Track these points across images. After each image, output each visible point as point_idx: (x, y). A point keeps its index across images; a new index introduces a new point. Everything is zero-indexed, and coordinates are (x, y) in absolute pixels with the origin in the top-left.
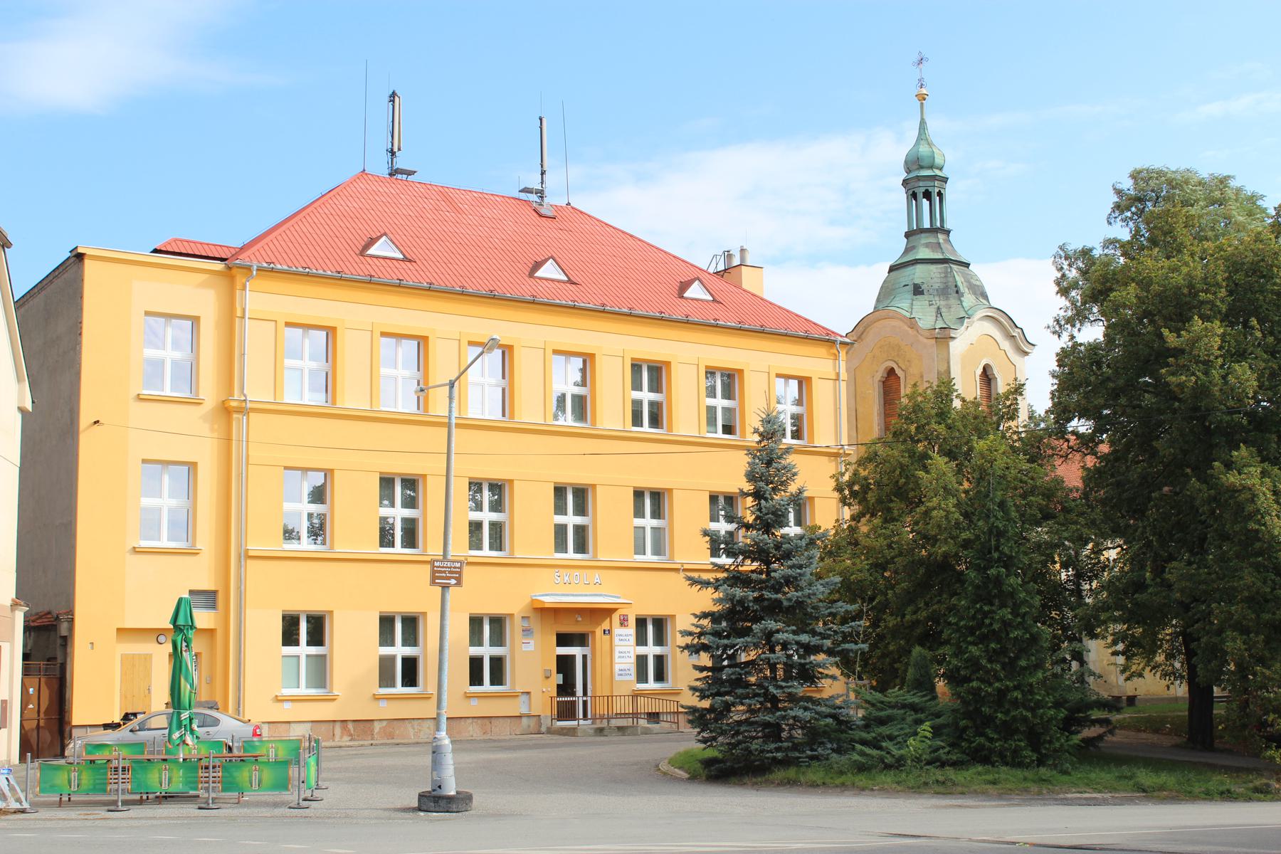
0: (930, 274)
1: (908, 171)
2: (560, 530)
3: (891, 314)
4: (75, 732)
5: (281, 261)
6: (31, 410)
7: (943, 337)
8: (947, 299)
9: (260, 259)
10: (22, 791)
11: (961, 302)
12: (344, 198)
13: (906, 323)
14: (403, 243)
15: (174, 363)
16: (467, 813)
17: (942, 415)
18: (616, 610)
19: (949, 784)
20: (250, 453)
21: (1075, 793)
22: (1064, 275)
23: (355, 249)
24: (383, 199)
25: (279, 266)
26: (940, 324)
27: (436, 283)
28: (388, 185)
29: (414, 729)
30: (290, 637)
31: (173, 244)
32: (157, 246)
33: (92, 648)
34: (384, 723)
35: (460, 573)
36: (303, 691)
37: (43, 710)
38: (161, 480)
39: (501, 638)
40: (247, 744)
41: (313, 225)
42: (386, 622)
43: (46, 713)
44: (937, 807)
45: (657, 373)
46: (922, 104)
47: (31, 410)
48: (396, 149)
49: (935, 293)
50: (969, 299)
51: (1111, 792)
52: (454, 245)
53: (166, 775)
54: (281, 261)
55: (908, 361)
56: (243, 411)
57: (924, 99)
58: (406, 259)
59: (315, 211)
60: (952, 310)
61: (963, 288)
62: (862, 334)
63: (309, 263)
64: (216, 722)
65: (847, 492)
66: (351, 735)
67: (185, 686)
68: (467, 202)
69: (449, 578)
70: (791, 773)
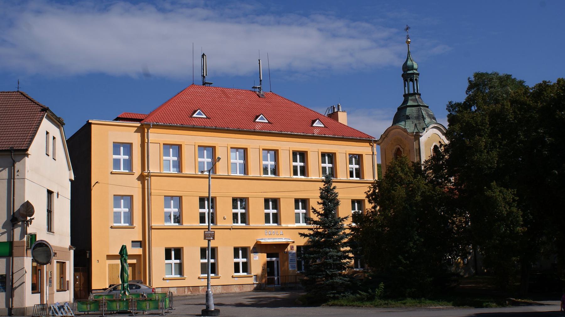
0: (412, 111)
1: (404, 71)
2: (267, 215)
3: (398, 127)
4: (93, 292)
5: (161, 121)
6: (74, 180)
7: (417, 136)
8: (419, 120)
11: (424, 121)
12: (186, 95)
13: (403, 130)
16: (218, 316)
19: (389, 304)
20: (152, 191)
22: (451, 113)
24: (200, 94)
25: (160, 124)
26: (416, 131)
27: (218, 126)
30: (168, 257)
31: (125, 115)
32: (119, 115)
34: (203, 287)
35: (214, 235)
36: (173, 276)
37: (81, 284)
38: (176, 171)
39: (246, 255)
40: (149, 294)
42: (236, 250)
43: (83, 285)
44: (381, 312)
45: (303, 156)
46: (408, 45)
47: (74, 180)
48: (205, 75)
49: (415, 118)
50: (427, 120)
51: (446, 306)
53: (118, 305)
54: (161, 121)
55: (405, 145)
56: (149, 175)
57: (409, 43)
58: (207, 118)
60: (421, 125)
61: (425, 116)
63: (172, 122)
64: (139, 287)
65: (371, 198)
66: (191, 292)
67: (125, 275)
69: (210, 237)
70: (336, 302)
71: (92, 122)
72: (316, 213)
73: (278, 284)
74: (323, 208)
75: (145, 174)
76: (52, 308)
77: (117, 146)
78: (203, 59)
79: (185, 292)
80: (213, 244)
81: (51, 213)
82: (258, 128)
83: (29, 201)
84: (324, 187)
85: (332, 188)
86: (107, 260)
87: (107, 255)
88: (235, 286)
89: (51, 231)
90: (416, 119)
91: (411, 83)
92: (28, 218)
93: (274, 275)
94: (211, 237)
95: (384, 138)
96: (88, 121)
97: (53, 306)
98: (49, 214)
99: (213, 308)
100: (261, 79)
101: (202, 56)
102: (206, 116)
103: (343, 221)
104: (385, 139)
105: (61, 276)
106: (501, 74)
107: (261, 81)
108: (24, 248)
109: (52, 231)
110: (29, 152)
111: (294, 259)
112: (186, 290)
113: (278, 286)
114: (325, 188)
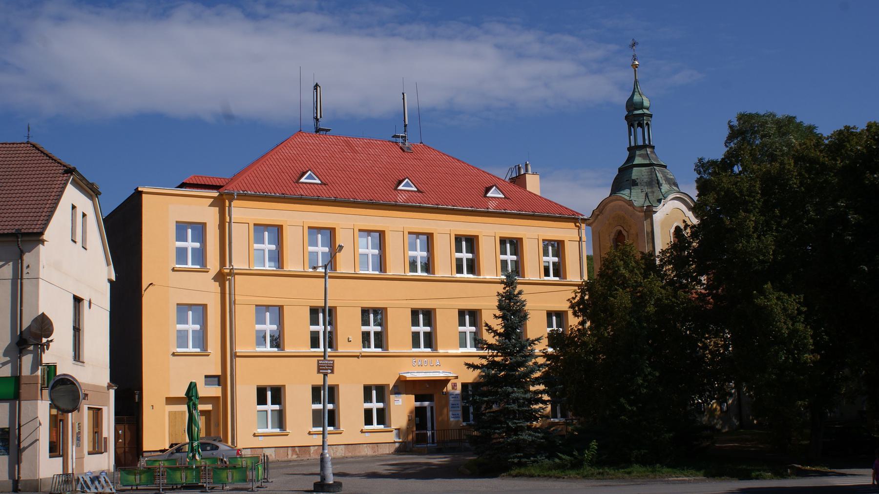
0: (642, 173)
2: (416, 336)
4: (145, 454)
5: (251, 189)
6: (115, 280)
7: (649, 213)
8: (652, 188)
9: (239, 188)
10: (111, 482)
11: (660, 189)
13: (627, 203)
14: (321, 174)
15: (193, 249)
16: (338, 493)
17: (503, 296)
18: (449, 380)
19: (605, 474)
20: (236, 298)
21: (674, 477)
23: (293, 179)
25: (249, 192)
28: (314, 138)
29: (333, 450)
30: (261, 400)
31: (193, 179)
33: (153, 409)
34: (316, 447)
35: (333, 367)
36: (270, 430)
37: (127, 442)
41: (270, 166)
42: (367, 390)
45: (472, 242)
46: (635, 70)
47: (115, 280)
48: (319, 117)
50: (665, 187)
51: (694, 476)
52: (351, 173)
54: (251, 189)
56: (232, 273)
58: (323, 184)
59: (271, 157)
60: (655, 194)
61: (662, 181)
62: (603, 209)
64: (217, 448)
65: (577, 309)
66: (297, 454)
67: (195, 429)
68: (361, 146)
69: (327, 369)
70: (522, 470)
71: (144, 191)
72: (491, 332)
73: (433, 442)
74: (503, 324)
75: (225, 271)
76: (81, 480)
77: (181, 228)
78: (315, 93)
79: (288, 454)
80: (331, 380)
81: (79, 332)
82: (401, 199)
83: (45, 313)
84: (504, 291)
85: (516, 292)
86: (166, 404)
87: (166, 398)
88: (366, 445)
89: (79, 361)
90: (647, 186)
91: (639, 130)
92: (44, 340)
93: (426, 429)
94: (329, 369)
95: (598, 215)
96: (137, 188)
97: (82, 477)
98: (77, 333)
99: (331, 480)
100: (407, 123)
101: (315, 87)
102: (321, 181)
103: (534, 344)
104: (599, 217)
105: (95, 431)
106: (780, 115)
107: (405, 126)
108: (38, 387)
109: (81, 360)
110: (45, 237)
111: (458, 404)
112: (290, 452)
113: (433, 445)
114: (505, 293)
